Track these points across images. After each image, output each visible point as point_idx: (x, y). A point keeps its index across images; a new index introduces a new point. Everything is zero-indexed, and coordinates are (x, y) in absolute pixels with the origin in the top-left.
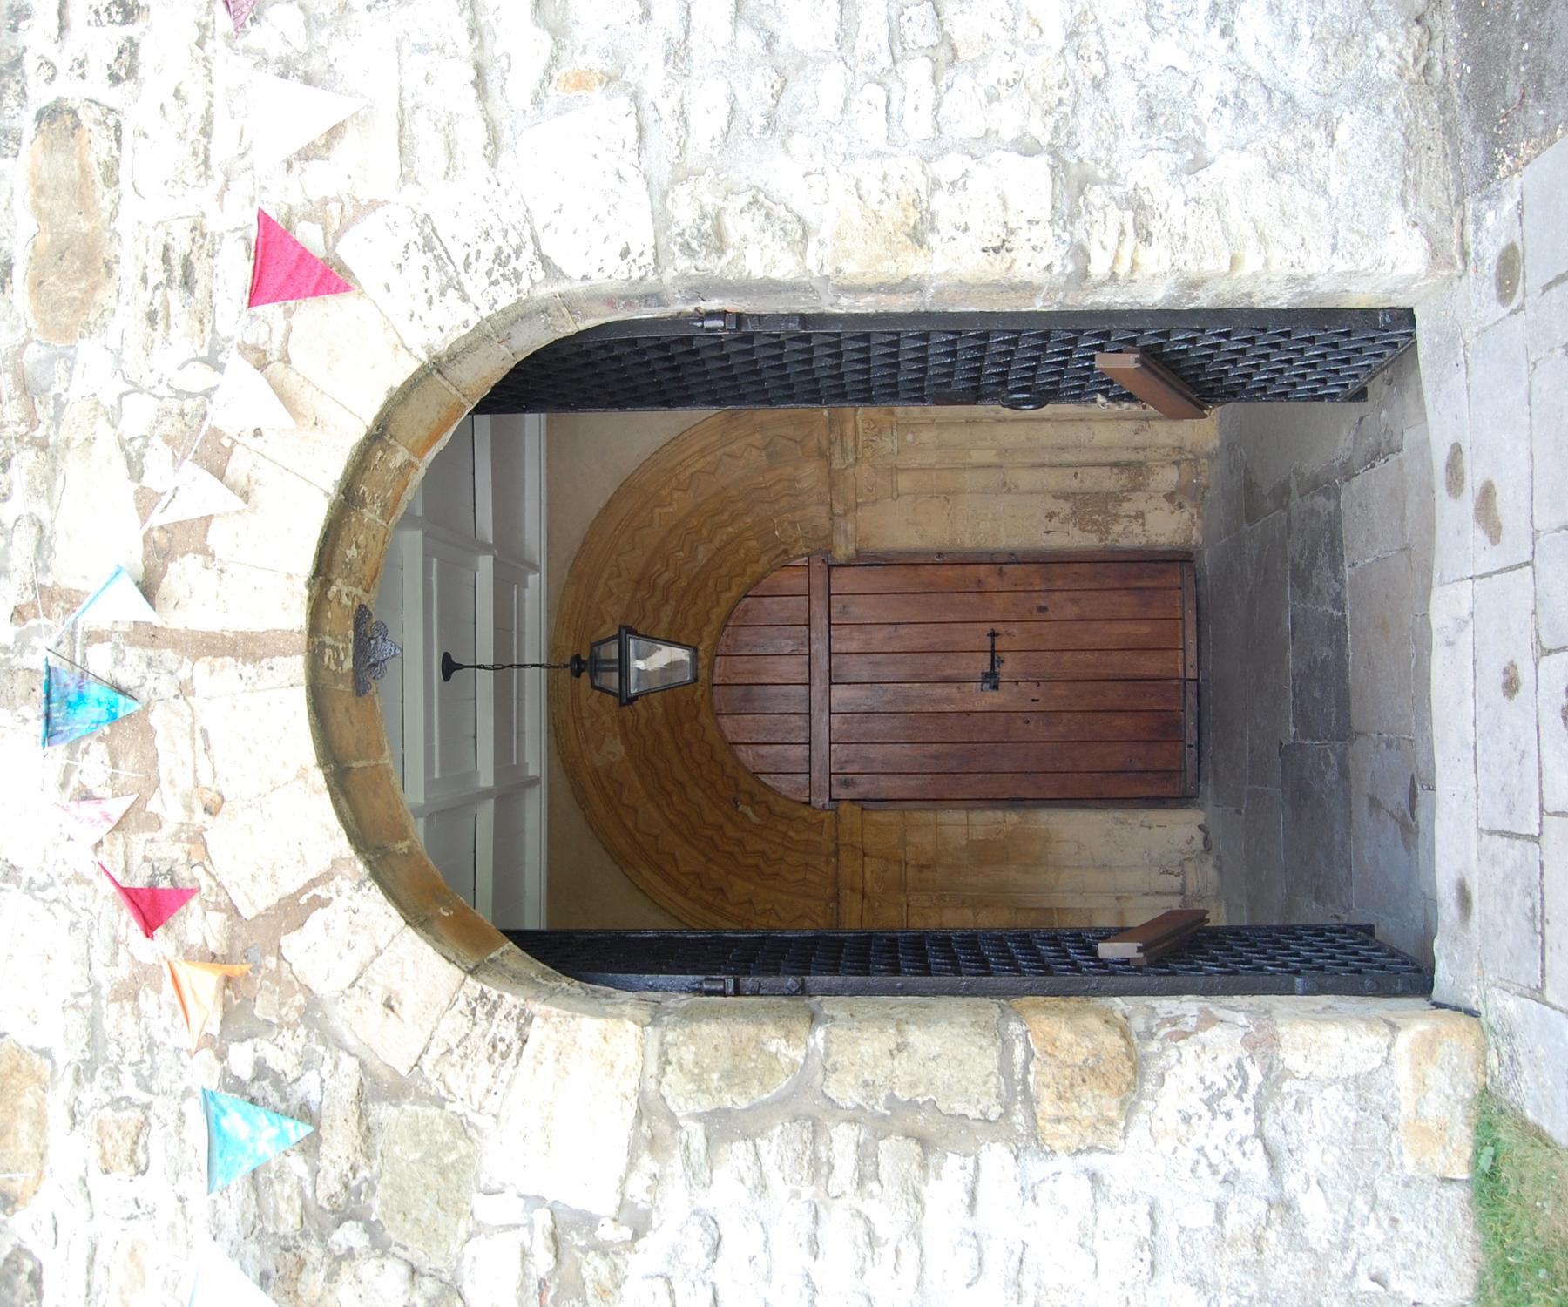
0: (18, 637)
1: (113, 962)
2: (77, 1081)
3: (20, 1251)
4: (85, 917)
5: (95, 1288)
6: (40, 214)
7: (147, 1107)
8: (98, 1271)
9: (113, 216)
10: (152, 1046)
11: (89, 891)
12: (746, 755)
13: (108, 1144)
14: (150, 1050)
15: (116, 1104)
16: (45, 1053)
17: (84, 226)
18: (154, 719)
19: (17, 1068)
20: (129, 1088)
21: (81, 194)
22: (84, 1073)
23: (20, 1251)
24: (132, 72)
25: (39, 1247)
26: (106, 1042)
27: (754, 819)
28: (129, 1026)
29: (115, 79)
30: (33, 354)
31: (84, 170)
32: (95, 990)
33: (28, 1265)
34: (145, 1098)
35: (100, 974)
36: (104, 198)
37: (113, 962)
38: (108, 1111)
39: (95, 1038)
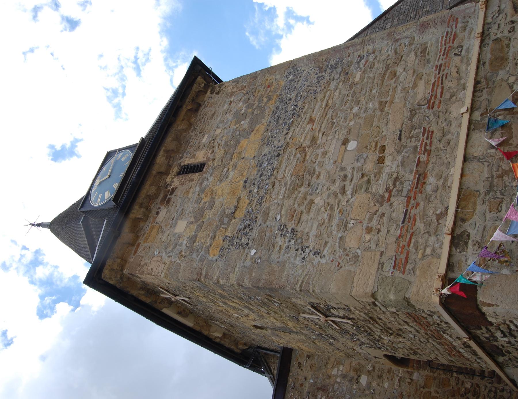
0: (481, 119)
1: (498, 171)
2: (485, 194)
3: (465, 231)
4: (492, 163)
5: (484, 236)
6: (492, 54)
7: (503, 198)
8: (485, 233)
9: (508, 53)
10: (505, 186)
11: (494, 158)
12: (484, 309)
13: (492, 206)
14: (505, 187)
15: (495, 198)
16: (478, 191)
17: (501, 55)
18: (512, 126)
19: (471, 194)
20: (498, 195)
21: (501, 50)
22: (487, 193)
23: (465, 231)
24: (513, 30)
25: (470, 231)
26: (494, 186)
27: (466, 355)
28: (500, 183)
29: (510, 32)
30: (489, 74)
31: (502, 46)
32: (492, 177)
33: (467, 233)
34: (502, 196)
35: (494, 174)
36: (506, 50)
37: (498, 171)
38: (493, 200)
39: (491, 186)
